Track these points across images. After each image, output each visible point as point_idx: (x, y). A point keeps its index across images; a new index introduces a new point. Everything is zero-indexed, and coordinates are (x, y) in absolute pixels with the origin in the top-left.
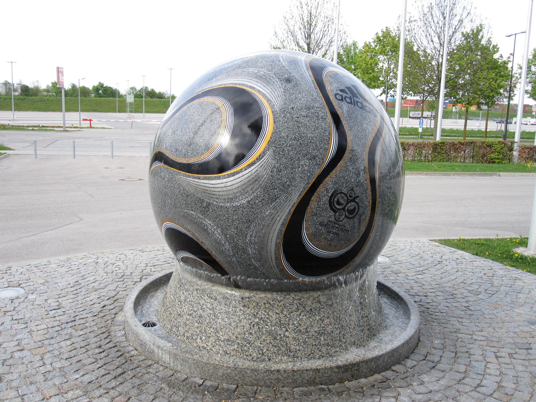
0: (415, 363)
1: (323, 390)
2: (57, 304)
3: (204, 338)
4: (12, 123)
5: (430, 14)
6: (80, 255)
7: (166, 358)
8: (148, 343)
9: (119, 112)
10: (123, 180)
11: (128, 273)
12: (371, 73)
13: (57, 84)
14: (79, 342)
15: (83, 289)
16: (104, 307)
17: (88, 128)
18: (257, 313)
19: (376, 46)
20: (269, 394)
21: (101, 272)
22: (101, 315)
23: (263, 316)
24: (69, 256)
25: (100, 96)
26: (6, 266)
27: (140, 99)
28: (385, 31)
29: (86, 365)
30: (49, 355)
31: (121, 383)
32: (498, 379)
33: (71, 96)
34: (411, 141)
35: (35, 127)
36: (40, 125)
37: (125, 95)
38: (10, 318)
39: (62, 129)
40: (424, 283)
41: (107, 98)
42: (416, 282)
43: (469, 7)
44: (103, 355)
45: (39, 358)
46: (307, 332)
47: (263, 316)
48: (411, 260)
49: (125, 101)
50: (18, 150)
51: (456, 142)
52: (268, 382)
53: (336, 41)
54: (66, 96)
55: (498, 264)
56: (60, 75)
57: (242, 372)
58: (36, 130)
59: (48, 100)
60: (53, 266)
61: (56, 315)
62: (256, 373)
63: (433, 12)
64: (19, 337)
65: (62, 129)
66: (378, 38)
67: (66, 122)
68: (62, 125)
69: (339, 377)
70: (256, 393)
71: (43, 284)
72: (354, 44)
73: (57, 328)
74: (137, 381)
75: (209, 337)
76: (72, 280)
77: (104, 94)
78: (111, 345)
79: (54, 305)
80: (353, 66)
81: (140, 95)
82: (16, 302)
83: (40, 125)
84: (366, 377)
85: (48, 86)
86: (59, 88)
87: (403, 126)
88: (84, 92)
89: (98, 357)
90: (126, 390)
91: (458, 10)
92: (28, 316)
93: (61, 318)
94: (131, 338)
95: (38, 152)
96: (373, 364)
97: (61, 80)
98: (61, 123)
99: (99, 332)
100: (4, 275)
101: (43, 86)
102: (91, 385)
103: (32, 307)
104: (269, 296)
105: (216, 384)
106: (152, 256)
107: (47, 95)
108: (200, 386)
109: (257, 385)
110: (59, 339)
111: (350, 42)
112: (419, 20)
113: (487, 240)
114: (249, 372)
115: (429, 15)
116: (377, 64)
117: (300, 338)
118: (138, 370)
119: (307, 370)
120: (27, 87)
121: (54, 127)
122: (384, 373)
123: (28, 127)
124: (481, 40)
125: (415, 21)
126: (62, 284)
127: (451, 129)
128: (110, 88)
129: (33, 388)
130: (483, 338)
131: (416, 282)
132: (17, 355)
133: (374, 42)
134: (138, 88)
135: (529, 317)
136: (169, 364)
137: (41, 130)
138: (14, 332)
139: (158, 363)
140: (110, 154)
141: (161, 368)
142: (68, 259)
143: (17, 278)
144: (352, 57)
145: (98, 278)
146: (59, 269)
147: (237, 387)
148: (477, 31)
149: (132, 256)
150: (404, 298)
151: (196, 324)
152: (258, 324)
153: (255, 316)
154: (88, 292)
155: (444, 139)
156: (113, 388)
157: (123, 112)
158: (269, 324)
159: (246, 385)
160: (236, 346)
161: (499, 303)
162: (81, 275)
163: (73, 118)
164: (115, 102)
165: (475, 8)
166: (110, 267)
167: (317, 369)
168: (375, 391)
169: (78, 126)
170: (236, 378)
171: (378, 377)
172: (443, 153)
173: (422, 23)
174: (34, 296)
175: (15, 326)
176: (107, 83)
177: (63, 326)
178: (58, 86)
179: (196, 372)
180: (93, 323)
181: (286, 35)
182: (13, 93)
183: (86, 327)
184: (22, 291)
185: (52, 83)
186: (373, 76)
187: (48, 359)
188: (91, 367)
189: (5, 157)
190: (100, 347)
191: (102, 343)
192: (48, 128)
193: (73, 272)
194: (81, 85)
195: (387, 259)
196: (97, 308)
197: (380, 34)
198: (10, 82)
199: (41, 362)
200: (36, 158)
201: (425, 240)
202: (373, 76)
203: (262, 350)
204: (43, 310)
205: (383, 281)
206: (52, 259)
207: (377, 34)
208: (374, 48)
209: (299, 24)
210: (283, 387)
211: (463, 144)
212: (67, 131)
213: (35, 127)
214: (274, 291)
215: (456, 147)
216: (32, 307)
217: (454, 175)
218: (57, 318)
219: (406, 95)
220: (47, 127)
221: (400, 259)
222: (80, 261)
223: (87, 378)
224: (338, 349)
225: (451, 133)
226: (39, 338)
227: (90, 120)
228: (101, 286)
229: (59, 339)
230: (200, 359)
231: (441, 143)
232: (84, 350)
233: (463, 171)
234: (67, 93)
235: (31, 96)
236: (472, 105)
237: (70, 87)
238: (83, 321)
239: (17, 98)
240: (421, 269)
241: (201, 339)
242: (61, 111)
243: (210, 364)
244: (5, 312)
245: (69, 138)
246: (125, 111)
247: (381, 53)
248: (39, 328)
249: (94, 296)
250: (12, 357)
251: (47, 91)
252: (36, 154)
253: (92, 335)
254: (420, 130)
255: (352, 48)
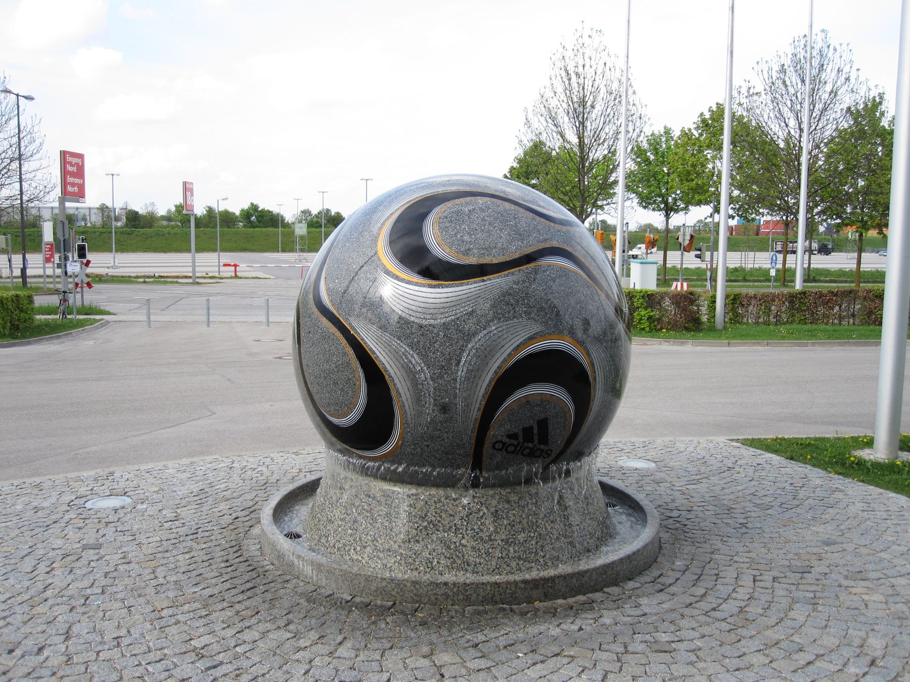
0: (638, 585)
1: (504, 609)
2: (175, 514)
3: (358, 548)
4: (111, 272)
5: (780, 81)
6: (209, 458)
7: (308, 570)
8: (287, 553)
9: (284, 251)
10: (280, 358)
11: (273, 480)
12: (693, 180)
13: (183, 207)
14: (200, 556)
15: (210, 499)
16: (236, 518)
17: (231, 278)
18: (426, 515)
19: (701, 135)
20: (433, 612)
21: (236, 478)
22: (232, 527)
23: (434, 519)
24: (194, 460)
25: (251, 225)
26: (107, 471)
27: (318, 230)
28: (715, 109)
29: (207, 579)
30: (162, 568)
31: (249, 598)
32: (743, 604)
33: (206, 226)
34: (751, 292)
35: (149, 277)
36: (157, 275)
37: (293, 223)
38: (114, 529)
39: (190, 281)
40: (694, 495)
41: (264, 229)
42: (684, 494)
43: (846, 69)
44: (229, 569)
45: (150, 571)
46: (492, 540)
47: (434, 519)
48: (689, 466)
49: (293, 232)
50: (122, 314)
51: (825, 291)
52: (433, 598)
53: (623, 133)
54: (197, 226)
55: (820, 471)
56: (188, 194)
57: (400, 584)
58: (149, 282)
59: (169, 233)
60: (170, 471)
61: (173, 527)
62: (417, 586)
63: (787, 79)
64: (125, 549)
65: (190, 281)
66: (704, 121)
67: (197, 269)
68: (191, 274)
69: (526, 594)
70: (416, 611)
71: (157, 492)
72: (667, 132)
73: (174, 541)
74: (269, 596)
75: (365, 547)
76: (195, 488)
77: (259, 222)
78: (241, 559)
79: (170, 516)
80: (665, 169)
81: (317, 222)
82: (121, 513)
83: (157, 275)
84: (565, 598)
85: (169, 211)
86: (186, 215)
87: (756, 266)
88: (227, 219)
89: (223, 571)
90: (254, 604)
91: (829, 75)
92: (136, 527)
93: (178, 530)
94: (267, 550)
95: (153, 318)
96: (574, 581)
97: (189, 203)
98: (188, 271)
99: (227, 546)
100: (105, 482)
101: (161, 211)
102: (213, 598)
103: (141, 518)
104: (441, 492)
105: (368, 600)
106: (310, 459)
107: (168, 226)
108: (347, 602)
109: (420, 602)
110: (175, 552)
111: (659, 129)
112: (763, 92)
113: (816, 439)
114: (409, 584)
115: (779, 83)
116: (703, 165)
117: (481, 547)
118: (272, 584)
119: (483, 584)
120: (135, 214)
121: (177, 277)
122: (590, 595)
123: (138, 277)
124: (880, 118)
125: (757, 94)
126: (182, 491)
127: (840, 270)
128: (269, 211)
129: (142, 600)
130: (748, 560)
131: (684, 494)
132: (121, 568)
133: (697, 128)
134: (315, 212)
135: (828, 536)
136: (312, 578)
137: (158, 282)
138: (118, 544)
139: (298, 578)
140: (263, 319)
141: (302, 584)
142: (192, 463)
143: (122, 484)
144: (663, 153)
145: (231, 485)
146: (179, 475)
147: (395, 604)
148: (873, 105)
149: (280, 460)
150: (645, 508)
151: (350, 531)
152: (426, 528)
153: (423, 518)
154: (216, 502)
155: (808, 287)
156: (239, 602)
157: (290, 251)
158: (441, 529)
159: (406, 602)
160: (399, 557)
161: (794, 519)
162: (209, 482)
163: (209, 262)
164: (276, 235)
165: (858, 70)
166: (249, 473)
167: (496, 583)
168: (571, 613)
169: (217, 275)
170: (393, 593)
171: (581, 598)
172: (805, 311)
173: (769, 97)
174: (145, 506)
175: (121, 538)
176: (264, 205)
177: (181, 539)
178: (185, 212)
179: (344, 587)
180: (220, 536)
181: (545, 124)
182: (114, 223)
183: (211, 540)
184: (129, 500)
185: (176, 206)
186: (697, 184)
187: (160, 572)
188: (214, 581)
189: (102, 325)
190: (227, 561)
191: (230, 557)
192: (169, 280)
193: (198, 478)
194: (221, 209)
195: (653, 465)
196: (227, 519)
197: (707, 115)
198: (110, 205)
199: (152, 576)
200: (150, 326)
201: (722, 439)
202: (697, 184)
203: (432, 563)
204: (156, 521)
205: (605, 480)
206: (170, 464)
207: (702, 114)
208: (697, 139)
209: (565, 105)
210: (452, 605)
211: (836, 295)
212: (198, 283)
213: (149, 277)
214: (449, 486)
215: (828, 299)
216: (141, 518)
217: (813, 344)
218: (174, 531)
219: (754, 216)
220: (167, 277)
221: (672, 464)
222: (208, 466)
223: (207, 592)
224: (533, 565)
225: (840, 276)
226: (150, 551)
227: (235, 266)
228: (235, 495)
229: (175, 552)
230: (349, 569)
231: (800, 294)
232: (207, 564)
233: (829, 338)
234: (199, 222)
235: (143, 228)
236: (868, 229)
237: (205, 212)
238: (207, 534)
239: (120, 232)
240: (698, 477)
241: (355, 549)
242: (189, 251)
243: (360, 575)
244: (107, 523)
245: (201, 296)
246: (292, 250)
247: (708, 147)
248: (150, 540)
249: (223, 506)
250: (116, 570)
251: (168, 218)
252: (149, 321)
253: (218, 549)
254: (773, 273)
255: (664, 139)
